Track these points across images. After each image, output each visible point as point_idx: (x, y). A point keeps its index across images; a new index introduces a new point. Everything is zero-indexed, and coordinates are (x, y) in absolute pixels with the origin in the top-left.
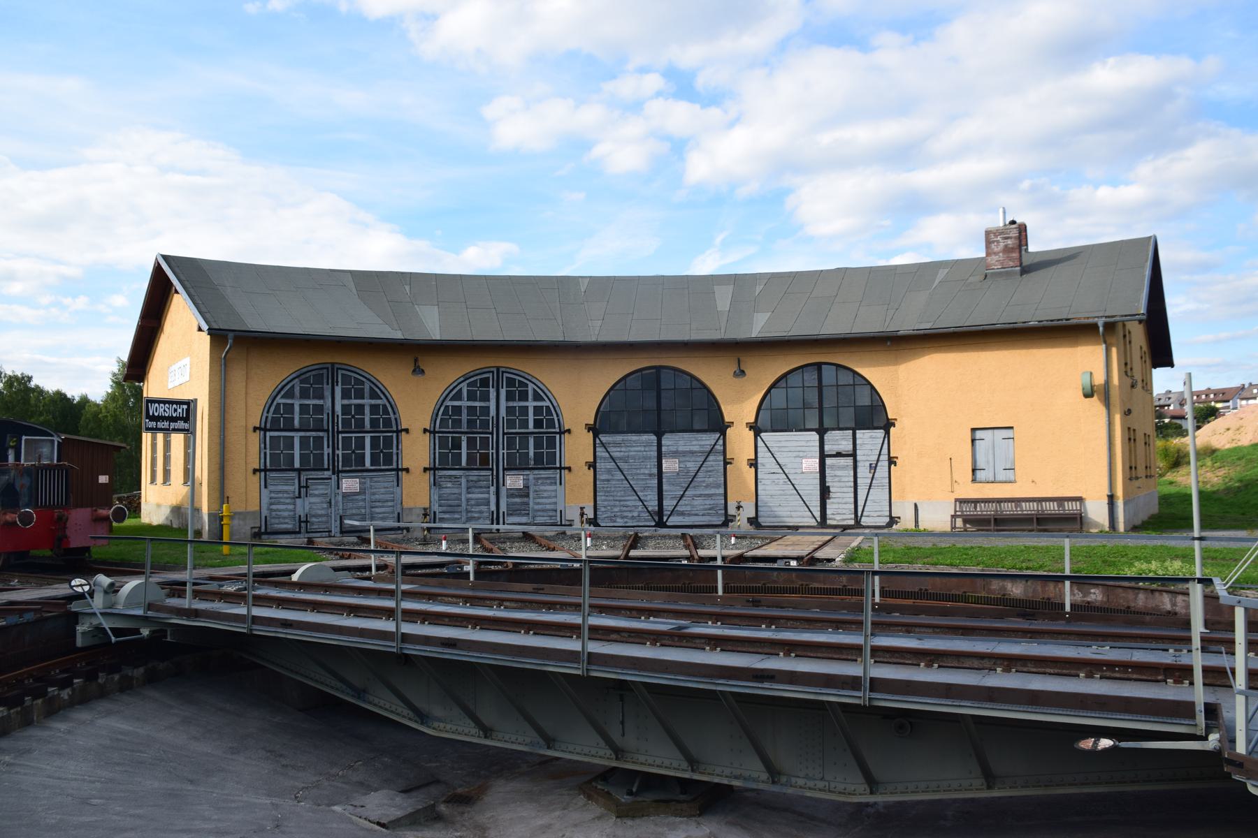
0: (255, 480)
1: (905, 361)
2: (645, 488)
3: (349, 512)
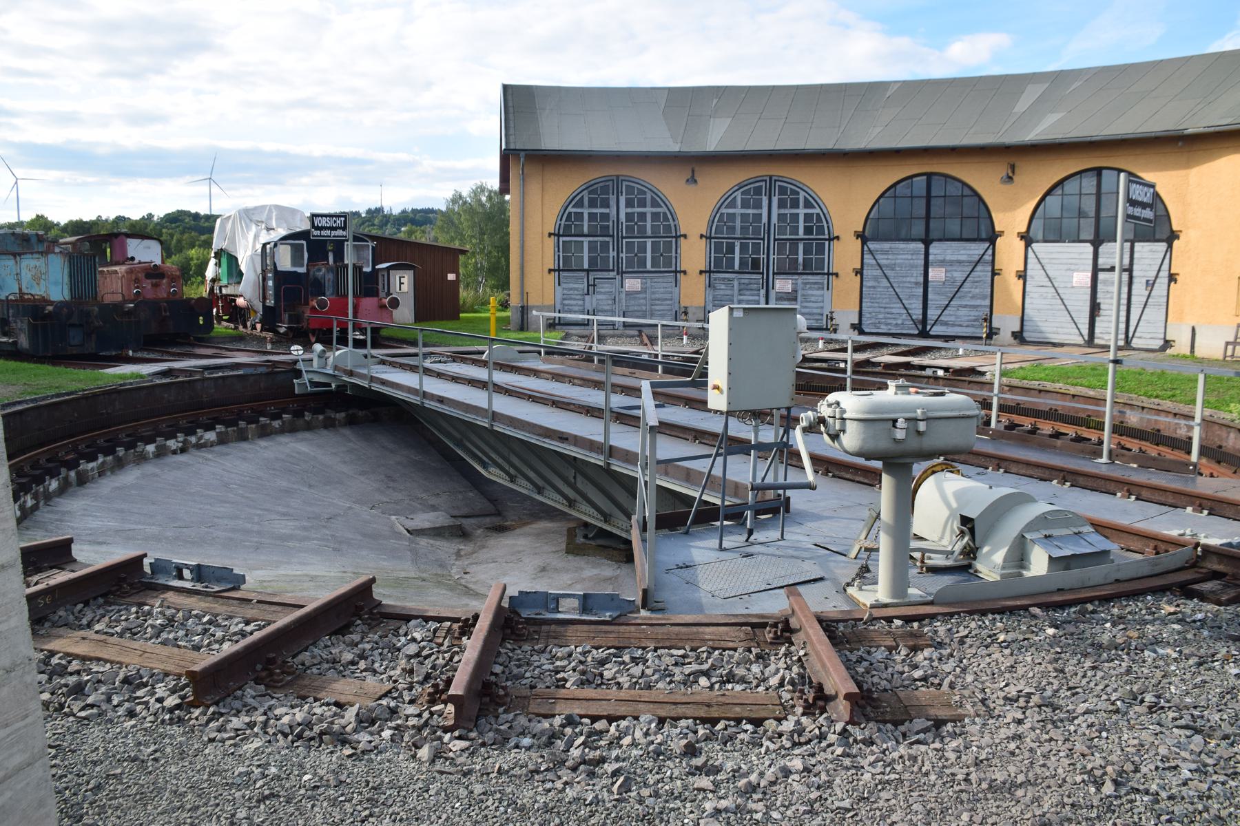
0: (550, 279)
1: (1198, 163)
2: (911, 296)
3: (631, 309)
